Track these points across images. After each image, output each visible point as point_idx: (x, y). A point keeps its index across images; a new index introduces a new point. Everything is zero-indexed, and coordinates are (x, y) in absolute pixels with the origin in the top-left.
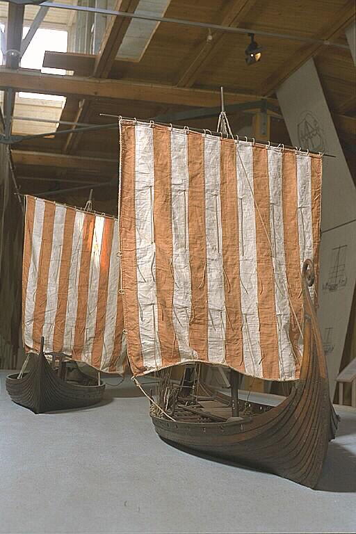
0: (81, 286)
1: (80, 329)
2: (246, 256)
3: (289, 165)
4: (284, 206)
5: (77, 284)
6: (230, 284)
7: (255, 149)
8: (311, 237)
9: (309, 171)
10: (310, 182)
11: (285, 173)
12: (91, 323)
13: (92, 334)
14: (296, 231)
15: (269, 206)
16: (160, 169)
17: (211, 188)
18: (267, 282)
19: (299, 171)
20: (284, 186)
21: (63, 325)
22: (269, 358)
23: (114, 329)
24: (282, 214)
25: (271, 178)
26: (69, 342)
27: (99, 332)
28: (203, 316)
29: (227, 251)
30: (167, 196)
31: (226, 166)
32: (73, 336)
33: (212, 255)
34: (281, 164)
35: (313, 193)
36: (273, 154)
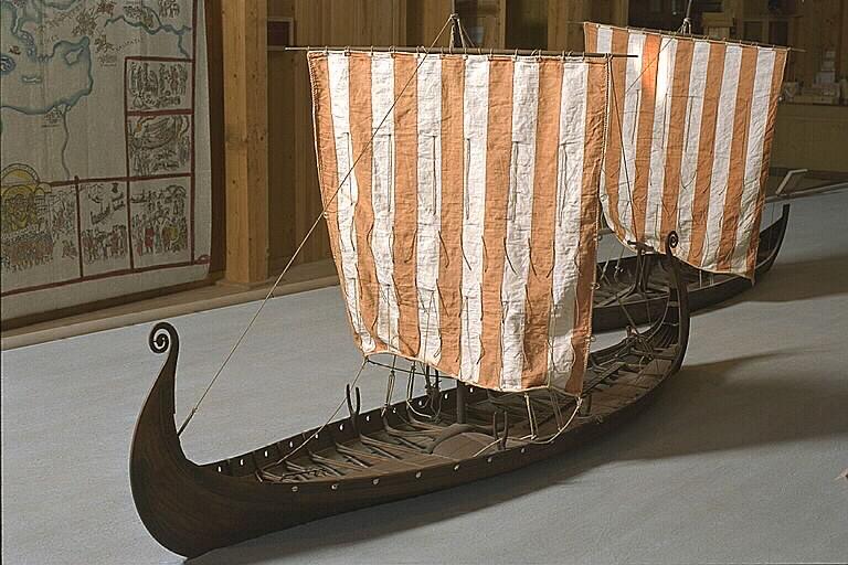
0: (672, 148)
1: (669, 206)
2: (471, 220)
3: (552, 80)
4: (539, 142)
5: (665, 145)
6: (449, 253)
7: (495, 64)
8: (580, 187)
9: (585, 84)
10: (585, 104)
11: (544, 95)
12: (687, 200)
13: (688, 216)
14: (554, 179)
15: (511, 147)
16: (358, 109)
17: (426, 128)
18: (494, 256)
19: (565, 89)
20: (541, 112)
21: (644, 203)
22: (491, 359)
23: (721, 209)
24: (533, 156)
25: (516, 105)
26: (653, 226)
27: (700, 215)
28: (411, 296)
29: (448, 211)
30: (365, 145)
31: (452, 93)
32: (660, 219)
33: (425, 217)
34: (536, 80)
35: (589, 121)
36: (523, 69)
